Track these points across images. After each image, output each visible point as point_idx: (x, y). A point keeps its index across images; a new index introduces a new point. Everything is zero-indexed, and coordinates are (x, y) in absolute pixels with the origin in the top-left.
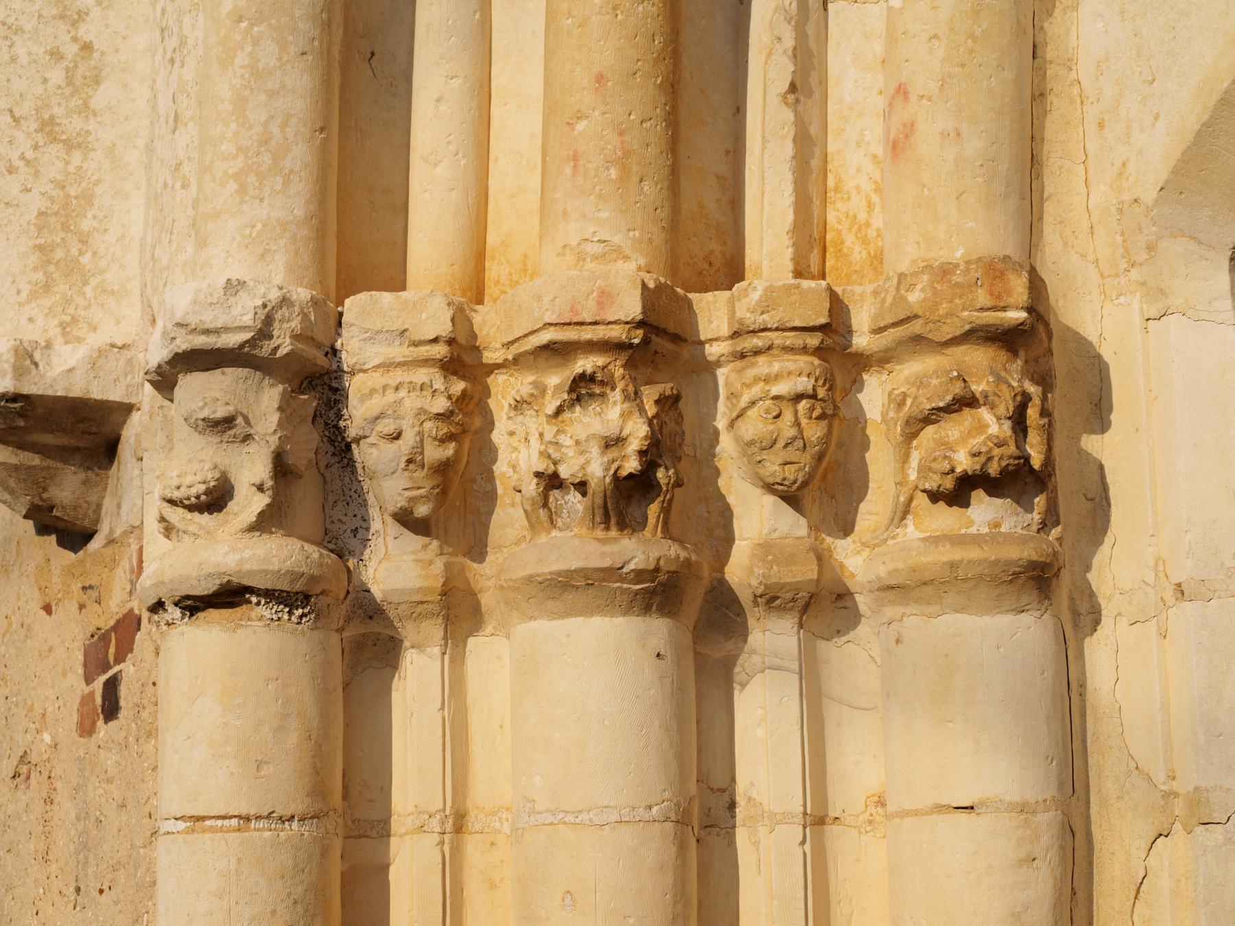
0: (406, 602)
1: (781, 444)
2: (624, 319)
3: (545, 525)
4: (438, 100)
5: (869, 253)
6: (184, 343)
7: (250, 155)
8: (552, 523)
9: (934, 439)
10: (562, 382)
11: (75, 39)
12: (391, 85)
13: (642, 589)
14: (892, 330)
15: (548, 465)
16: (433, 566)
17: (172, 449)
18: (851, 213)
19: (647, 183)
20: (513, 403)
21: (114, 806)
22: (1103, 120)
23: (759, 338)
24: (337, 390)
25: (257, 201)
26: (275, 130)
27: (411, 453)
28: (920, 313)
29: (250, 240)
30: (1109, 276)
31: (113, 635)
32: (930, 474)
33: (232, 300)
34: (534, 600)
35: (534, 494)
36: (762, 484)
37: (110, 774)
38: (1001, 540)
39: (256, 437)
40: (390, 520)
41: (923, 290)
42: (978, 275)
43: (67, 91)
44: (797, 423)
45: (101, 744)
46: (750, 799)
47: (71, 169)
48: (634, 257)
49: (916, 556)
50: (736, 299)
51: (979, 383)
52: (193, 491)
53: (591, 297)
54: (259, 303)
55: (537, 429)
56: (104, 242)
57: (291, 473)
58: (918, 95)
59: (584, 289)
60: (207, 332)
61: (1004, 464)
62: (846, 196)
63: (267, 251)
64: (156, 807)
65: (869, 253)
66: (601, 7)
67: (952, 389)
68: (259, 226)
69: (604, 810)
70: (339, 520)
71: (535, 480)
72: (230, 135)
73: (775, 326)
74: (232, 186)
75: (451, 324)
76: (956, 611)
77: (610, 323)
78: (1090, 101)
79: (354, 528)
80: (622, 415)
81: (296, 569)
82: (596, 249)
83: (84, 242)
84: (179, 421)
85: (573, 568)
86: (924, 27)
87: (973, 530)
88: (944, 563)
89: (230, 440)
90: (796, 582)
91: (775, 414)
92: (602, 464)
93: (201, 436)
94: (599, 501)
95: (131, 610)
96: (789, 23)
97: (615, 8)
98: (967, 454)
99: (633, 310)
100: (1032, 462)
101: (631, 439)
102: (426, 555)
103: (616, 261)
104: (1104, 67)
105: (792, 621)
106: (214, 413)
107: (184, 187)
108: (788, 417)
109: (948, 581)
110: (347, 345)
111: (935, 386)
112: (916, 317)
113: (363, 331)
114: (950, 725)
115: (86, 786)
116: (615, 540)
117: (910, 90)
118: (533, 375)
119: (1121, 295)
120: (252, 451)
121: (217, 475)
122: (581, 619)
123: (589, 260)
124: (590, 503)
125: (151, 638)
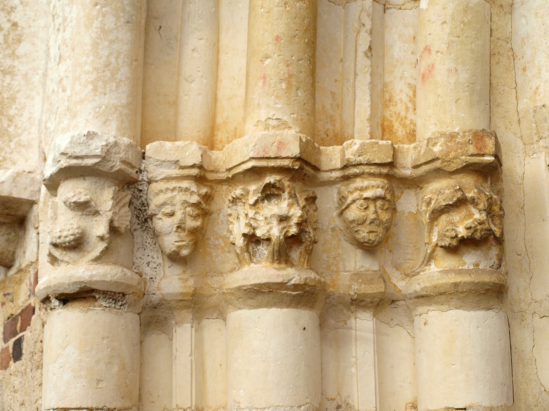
0: (174, 300)
1: (368, 222)
2: (290, 156)
3: (247, 261)
4: (193, 50)
5: (406, 132)
6: (65, 163)
7: (100, 71)
8: (251, 260)
9: (446, 221)
10: (258, 188)
11: (9, 21)
12: (169, 43)
13: (297, 294)
14: (424, 166)
15: (250, 230)
16: (188, 282)
17: (56, 219)
18: (397, 112)
19: (300, 91)
20: (231, 199)
21: (18, 404)
22: (526, 67)
23: (357, 168)
24: (141, 191)
25: (103, 95)
26: (113, 60)
27: (179, 223)
28: (440, 157)
29: (99, 114)
30: (528, 144)
31: (20, 318)
32: (445, 238)
33: (90, 142)
34: (241, 299)
35: (242, 245)
36: (356, 243)
37: (16, 388)
38: (480, 272)
39: (101, 213)
40: (166, 259)
41: (441, 145)
42: (470, 138)
43: (4, 46)
44: (376, 212)
45: (12, 373)
46: (348, 404)
47: (5, 84)
48: (294, 127)
49: (437, 280)
50: (345, 149)
51: (469, 193)
52: (67, 239)
53: (274, 145)
54: (104, 143)
55: (244, 212)
56: (20, 121)
57: (118, 232)
58: (436, 51)
59: (270, 141)
60: (77, 157)
61: (482, 233)
62: (394, 104)
63: (107, 120)
64: (41, 404)
65: (406, 132)
66: (279, 3)
67: (456, 195)
68: (103, 108)
69: (277, 408)
70: (140, 258)
71: (243, 238)
72: (89, 61)
73: (365, 162)
74: (90, 87)
75: (201, 158)
76: (457, 308)
77: (284, 158)
78: (518, 58)
79: (148, 262)
80: (288, 205)
81: (119, 281)
82: (275, 123)
83: (10, 121)
84: (61, 204)
85: (262, 283)
86: (439, 18)
87: (466, 267)
88: (452, 284)
89: (87, 213)
90: (373, 293)
91: (365, 207)
92: (278, 230)
93: (72, 212)
94: (276, 248)
95: (30, 304)
96: (369, 17)
97: (286, 4)
98: (464, 228)
99: (296, 152)
100: (496, 233)
101: (293, 217)
102: (185, 276)
103: (284, 129)
104: (526, 41)
105: (370, 313)
106: (79, 199)
107: (64, 91)
108: (372, 208)
109: (453, 293)
110: (148, 168)
111: (448, 194)
112: (438, 159)
113: (156, 161)
114: (454, 366)
115: (3, 395)
116: (284, 269)
117: (432, 48)
118: (242, 185)
119: (534, 153)
120: (98, 220)
121: (80, 231)
122: (265, 309)
123: (270, 128)
124: (271, 249)
125: (40, 318)
